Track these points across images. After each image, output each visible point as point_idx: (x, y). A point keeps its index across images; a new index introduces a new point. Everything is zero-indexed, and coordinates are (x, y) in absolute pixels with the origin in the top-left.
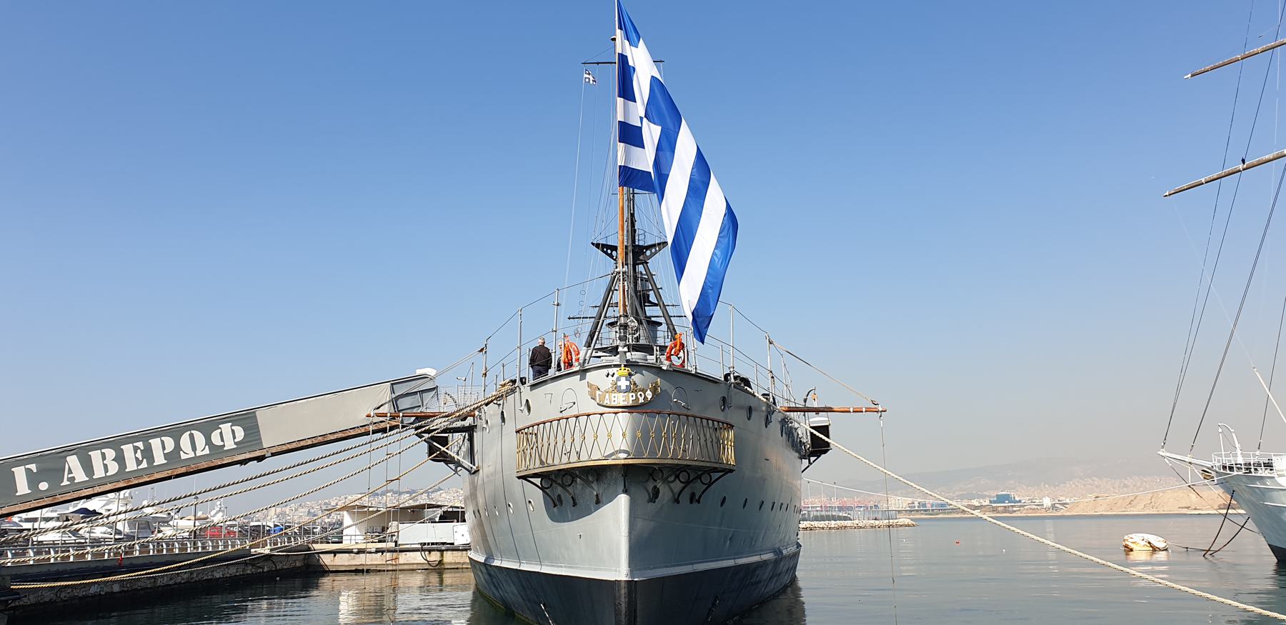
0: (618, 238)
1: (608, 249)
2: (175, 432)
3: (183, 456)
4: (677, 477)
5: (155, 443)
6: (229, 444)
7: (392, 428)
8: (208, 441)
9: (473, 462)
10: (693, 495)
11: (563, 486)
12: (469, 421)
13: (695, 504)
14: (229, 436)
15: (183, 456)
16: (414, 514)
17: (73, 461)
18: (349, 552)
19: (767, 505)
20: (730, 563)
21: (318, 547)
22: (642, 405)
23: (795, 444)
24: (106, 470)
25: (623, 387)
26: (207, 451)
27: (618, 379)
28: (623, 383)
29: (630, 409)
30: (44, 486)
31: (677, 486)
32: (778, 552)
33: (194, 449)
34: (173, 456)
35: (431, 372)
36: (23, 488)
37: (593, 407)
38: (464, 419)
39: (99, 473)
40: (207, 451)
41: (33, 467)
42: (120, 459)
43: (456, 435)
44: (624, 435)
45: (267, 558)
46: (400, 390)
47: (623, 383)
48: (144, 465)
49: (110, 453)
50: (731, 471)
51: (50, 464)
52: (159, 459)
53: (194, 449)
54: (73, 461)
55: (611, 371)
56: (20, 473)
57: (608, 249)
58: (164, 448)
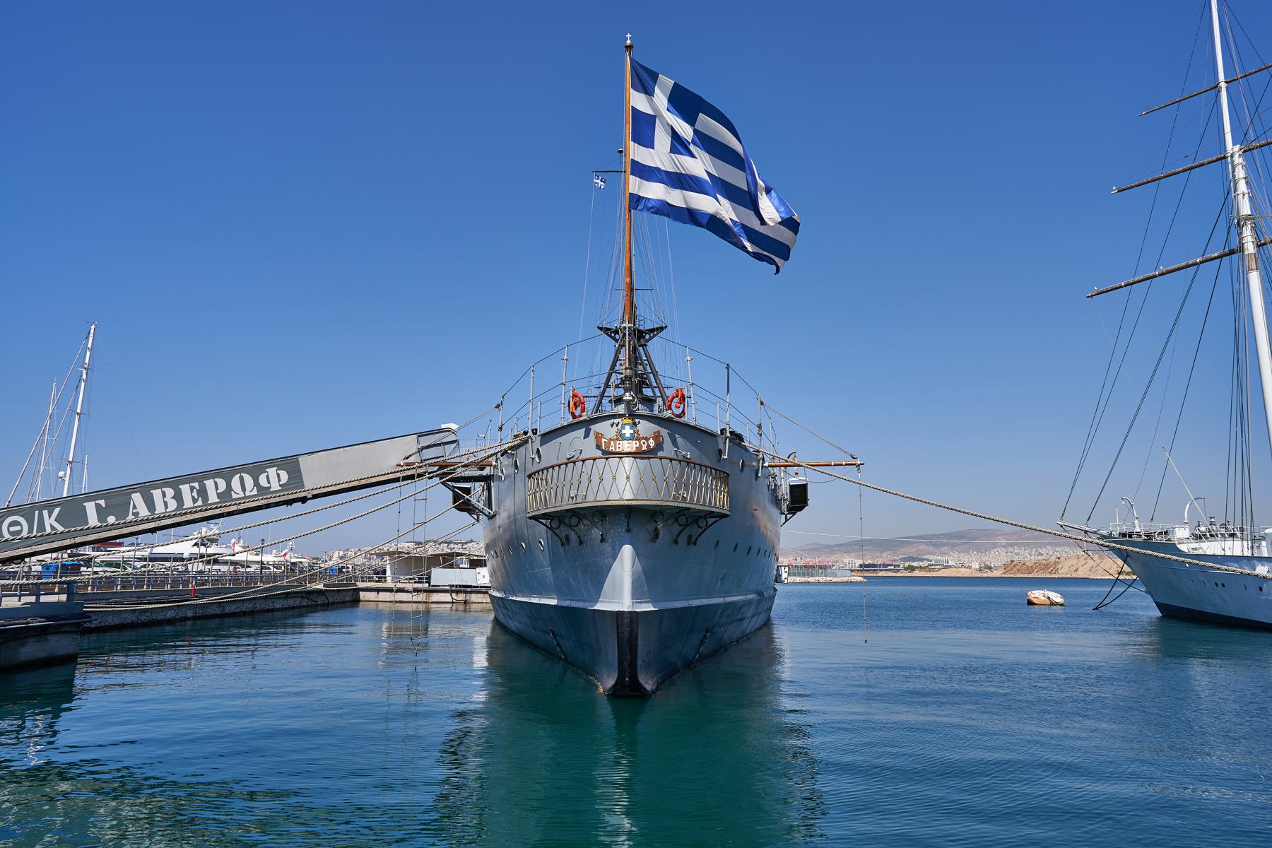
0: (616, 319)
1: (610, 332)
2: (226, 473)
3: (234, 496)
4: (677, 520)
5: (209, 484)
6: (275, 486)
7: (420, 475)
8: (256, 484)
9: (490, 507)
10: (690, 537)
11: (570, 526)
12: (487, 471)
13: (692, 547)
14: (275, 479)
15: (234, 496)
16: (448, 560)
17: (137, 498)
18: (390, 590)
19: (754, 551)
20: (721, 600)
21: (361, 585)
22: (644, 452)
23: (777, 502)
24: (166, 507)
25: (628, 435)
26: (255, 492)
27: (623, 427)
28: (628, 431)
29: (636, 455)
30: (111, 520)
31: (676, 529)
32: (760, 594)
33: (244, 489)
34: (225, 496)
35: (454, 426)
36: (93, 520)
37: (599, 453)
38: (482, 469)
39: (160, 509)
40: (255, 492)
41: (102, 502)
42: (178, 497)
43: (477, 484)
44: (628, 478)
45: (319, 592)
46: (426, 441)
47: (628, 431)
48: (200, 503)
49: (170, 492)
50: (726, 516)
51: (116, 499)
52: (213, 498)
53: (244, 489)
54: (137, 498)
55: (616, 421)
56: (90, 507)
57: (610, 332)
58: (217, 488)
